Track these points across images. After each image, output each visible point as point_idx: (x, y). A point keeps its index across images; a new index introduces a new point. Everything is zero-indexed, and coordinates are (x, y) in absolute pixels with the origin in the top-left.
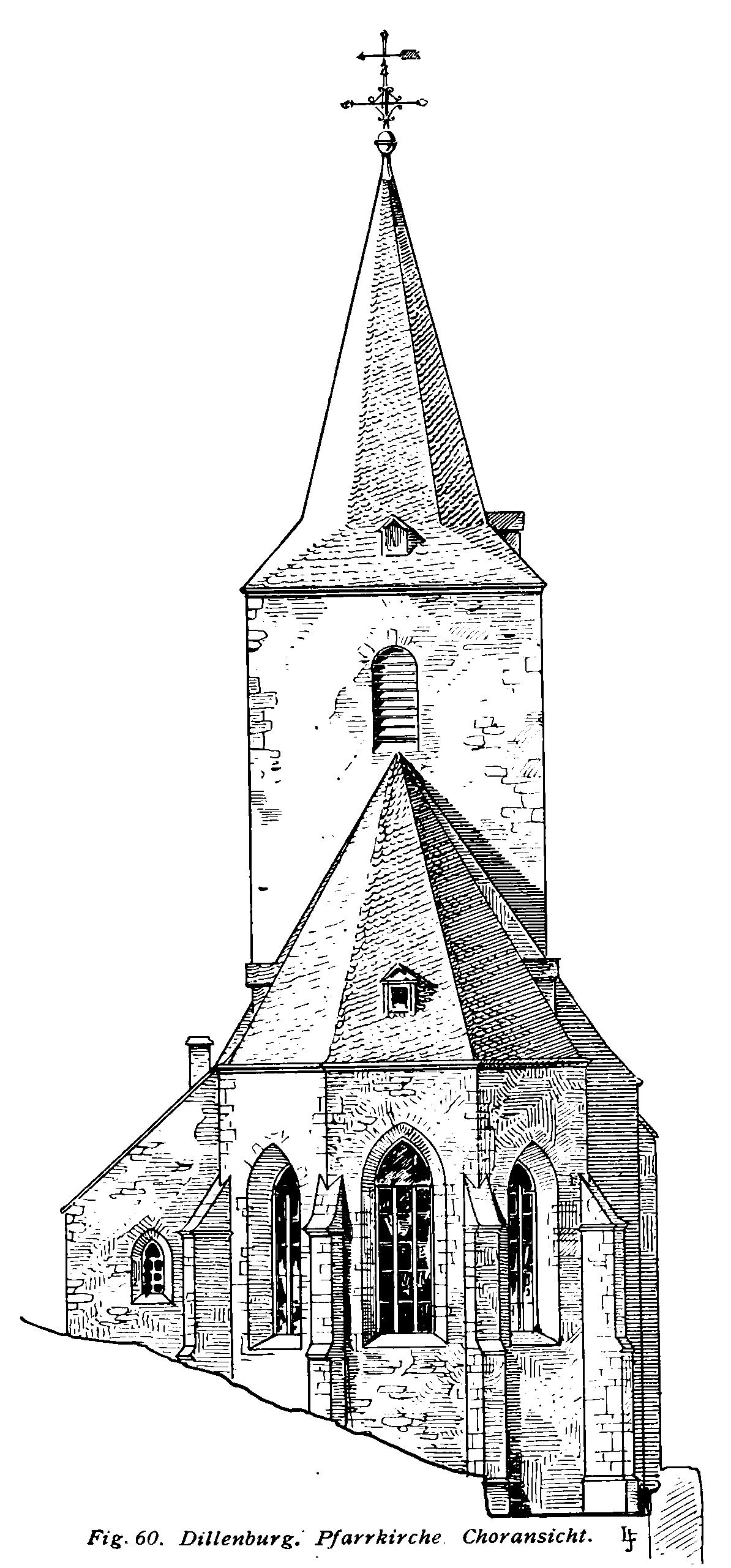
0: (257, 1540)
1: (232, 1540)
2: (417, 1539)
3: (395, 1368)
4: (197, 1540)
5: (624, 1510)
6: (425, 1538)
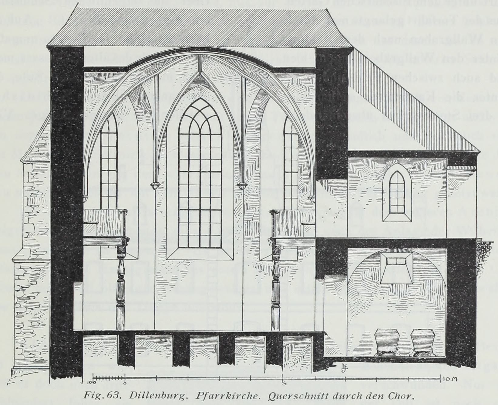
0: (167, 396)
1: (378, 397)
2: (245, 397)
3: (287, 117)
4: (138, 396)
5: (220, 211)
6: (250, 396)
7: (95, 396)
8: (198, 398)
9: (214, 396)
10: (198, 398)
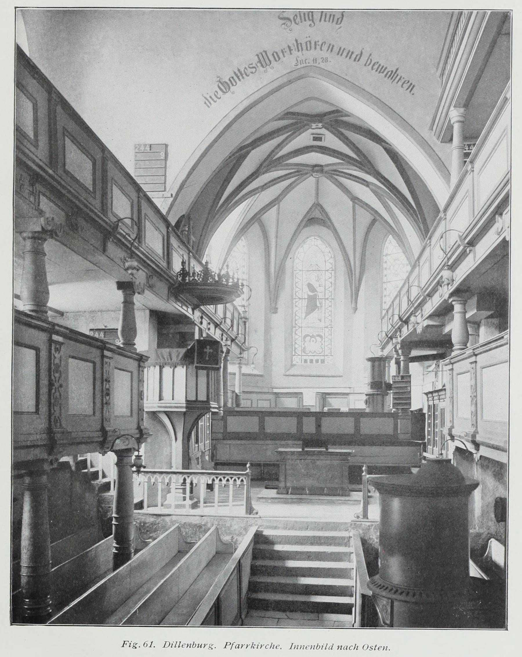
0: (197, 646)
2: (268, 647)
4: (171, 645)
6: (272, 646)
7: (132, 645)
8: (123, 646)
9: (240, 646)
10: (123, 646)
